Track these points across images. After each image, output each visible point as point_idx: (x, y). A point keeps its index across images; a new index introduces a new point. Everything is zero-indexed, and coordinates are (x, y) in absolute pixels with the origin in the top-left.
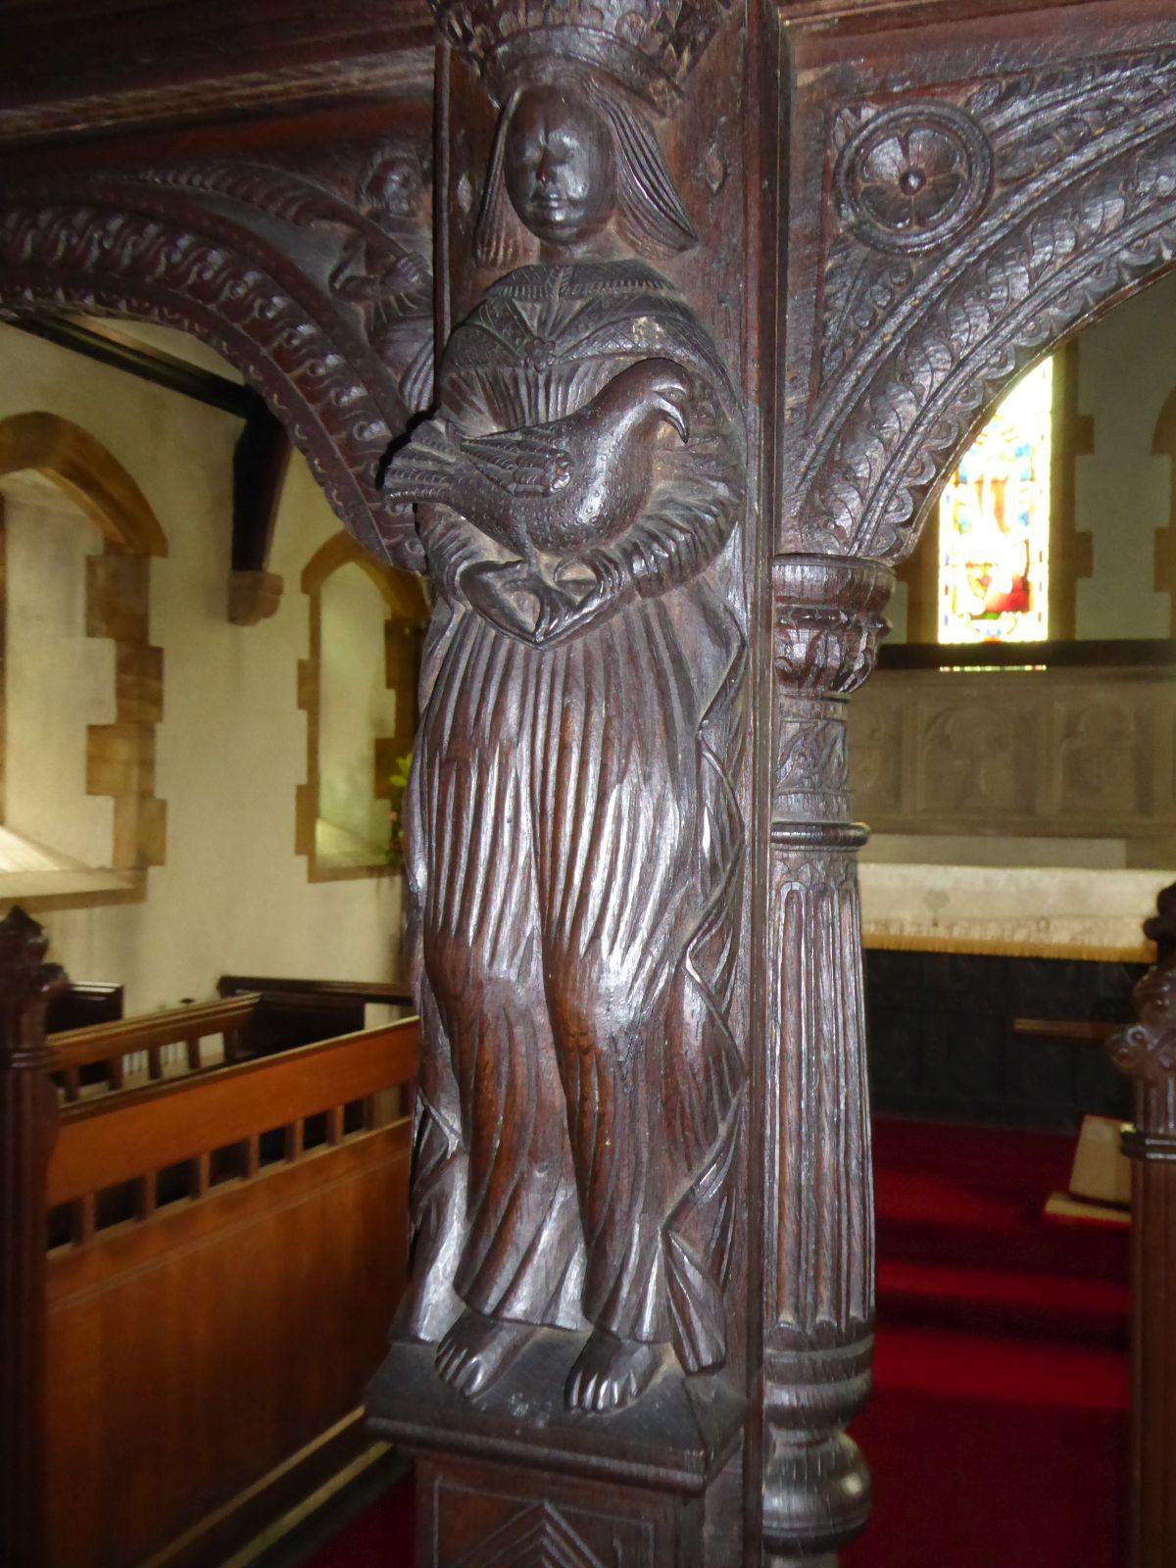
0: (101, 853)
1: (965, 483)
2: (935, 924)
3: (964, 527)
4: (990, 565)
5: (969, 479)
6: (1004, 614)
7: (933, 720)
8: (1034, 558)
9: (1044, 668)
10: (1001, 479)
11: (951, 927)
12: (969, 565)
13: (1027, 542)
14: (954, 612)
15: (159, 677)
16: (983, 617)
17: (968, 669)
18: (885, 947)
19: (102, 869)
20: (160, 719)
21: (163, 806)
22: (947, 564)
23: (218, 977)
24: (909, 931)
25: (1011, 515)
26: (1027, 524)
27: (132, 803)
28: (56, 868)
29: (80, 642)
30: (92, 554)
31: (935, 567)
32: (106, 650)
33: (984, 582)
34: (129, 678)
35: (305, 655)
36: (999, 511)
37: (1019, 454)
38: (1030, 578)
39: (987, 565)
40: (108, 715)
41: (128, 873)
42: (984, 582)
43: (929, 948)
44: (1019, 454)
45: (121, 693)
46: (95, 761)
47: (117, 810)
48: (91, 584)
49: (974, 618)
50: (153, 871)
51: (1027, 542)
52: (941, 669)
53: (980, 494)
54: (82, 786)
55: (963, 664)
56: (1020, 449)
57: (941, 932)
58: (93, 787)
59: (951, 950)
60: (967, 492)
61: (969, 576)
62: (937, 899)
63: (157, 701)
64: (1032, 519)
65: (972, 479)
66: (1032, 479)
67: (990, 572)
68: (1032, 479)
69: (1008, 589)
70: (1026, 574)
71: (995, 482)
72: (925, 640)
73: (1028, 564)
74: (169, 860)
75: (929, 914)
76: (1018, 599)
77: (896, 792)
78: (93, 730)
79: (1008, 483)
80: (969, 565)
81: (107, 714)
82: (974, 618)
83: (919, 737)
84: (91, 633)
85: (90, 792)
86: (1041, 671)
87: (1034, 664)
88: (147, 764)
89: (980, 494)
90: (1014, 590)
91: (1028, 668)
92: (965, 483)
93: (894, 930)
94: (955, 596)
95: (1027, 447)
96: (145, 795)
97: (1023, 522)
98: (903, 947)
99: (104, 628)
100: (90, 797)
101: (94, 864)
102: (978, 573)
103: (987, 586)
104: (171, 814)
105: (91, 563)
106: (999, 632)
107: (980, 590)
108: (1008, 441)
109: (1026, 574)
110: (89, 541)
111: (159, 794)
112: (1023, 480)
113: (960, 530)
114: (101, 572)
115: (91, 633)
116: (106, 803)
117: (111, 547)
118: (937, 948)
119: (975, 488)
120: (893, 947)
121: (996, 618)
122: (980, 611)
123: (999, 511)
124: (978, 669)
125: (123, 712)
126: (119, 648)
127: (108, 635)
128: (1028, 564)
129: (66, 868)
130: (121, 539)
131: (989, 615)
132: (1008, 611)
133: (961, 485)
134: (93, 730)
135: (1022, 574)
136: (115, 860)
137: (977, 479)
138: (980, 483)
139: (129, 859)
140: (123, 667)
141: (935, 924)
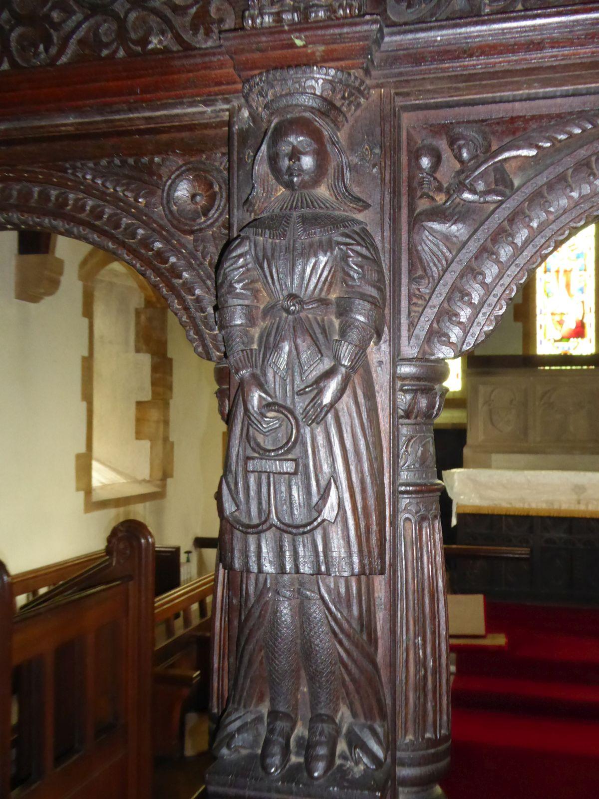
0: (144, 472)
1: (550, 271)
2: (579, 503)
3: (550, 295)
4: (564, 314)
5: (551, 270)
6: (572, 339)
7: (545, 393)
8: (587, 311)
9: (593, 367)
10: (569, 269)
11: (587, 505)
12: (553, 314)
13: (583, 302)
14: (545, 338)
15: (171, 375)
16: (560, 340)
17: (553, 368)
18: (552, 515)
19: (144, 481)
20: (171, 398)
21: (172, 444)
22: (541, 313)
23: (194, 538)
24: (565, 507)
25: (574, 288)
26: (583, 293)
27: (160, 442)
28: (125, 481)
29: (132, 355)
30: (138, 307)
31: (535, 316)
32: (146, 360)
33: (561, 323)
34: (158, 375)
35: (86, 354)
36: (568, 286)
37: (578, 257)
38: (585, 321)
39: (562, 314)
40: (147, 396)
41: (158, 482)
42: (561, 323)
43: (576, 516)
44: (578, 257)
45: (153, 384)
46: (140, 421)
47: (151, 447)
48: (137, 323)
49: (555, 341)
50: (169, 481)
51: (583, 302)
52: (539, 368)
53: (558, 278)
54: (134, 435)
55: (550, 365)
56: (578, 254)
57: (582, 507)
58: (139, 435)
59: (588, 516)
60: (551, 276)
61: (553, 319)
62: (579, 489)
63: (170, 388)
64: (585, 290)
65: (553, 270)
66: (585, 270)
67: (564, 318)
68: (585, 270)
69: (573, 326)
70: (583, 318)
71: (566, 271)
72: (531, 353)
73: (584, 314)
74: (175, 474)
75: (575, 497)
76: (579, 332)
77: (525, 431)
78: (139, 404)
79: (572, 273)
80: (553, 314)
81: (146, 395)
82: (555, 341)
83: (537, 403)
84: (138, 350)
85: (137, 438)
86: (592, 369)
87: (588, 365)
88: (166, 423)
89: (558, 278)
90: (577, 327)
91: (547, 368)
92: (550, 271)
93: (556, 506)
94: (545, 330)
95: (582, 253)
96: (166, 439)
97: (581, 292)
98: (562, 515)
99: (144, 347)
100: (138, 441)
101: (140, 478)
102: (558, 318)
103: (562, 324)
104: (175, 447)
105: (138, 313)
106: (569, 349)
107: (559, 326)
108: (572, 250)
109: (583, 318)
110: (137, 300)
111: (171, 439)
112: (580, 270)
113: (548, 296)
114: (143, 317)
115: (138, 350)
116: (146, 444)
117: (148, 303)
118: (580, 515)
119: (555, 274)
120: (556, 515)
121: (567, 341)
122: (559, 338)
123: (568, 286)
124: (569, 368)
125: (154, 393)
126: (152, 358)
127: (147, 352)
128: (584, 314)
129: (129, 481)
130: (154, 299)
131: (564, 340)
132: (574, 338)
133: (548, 273)
134: (139, 404)
135: (581, 319)
136: (151, 476)
137: (556, 269)
138: (558, 272)
139: (159, 475)
140: (155, 369)
141: (579, 503)
